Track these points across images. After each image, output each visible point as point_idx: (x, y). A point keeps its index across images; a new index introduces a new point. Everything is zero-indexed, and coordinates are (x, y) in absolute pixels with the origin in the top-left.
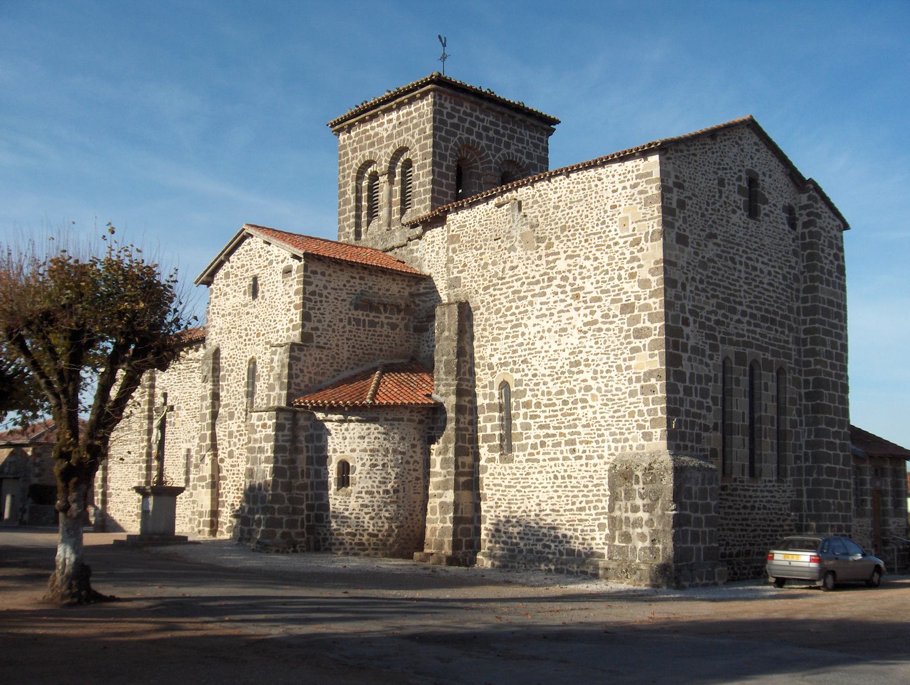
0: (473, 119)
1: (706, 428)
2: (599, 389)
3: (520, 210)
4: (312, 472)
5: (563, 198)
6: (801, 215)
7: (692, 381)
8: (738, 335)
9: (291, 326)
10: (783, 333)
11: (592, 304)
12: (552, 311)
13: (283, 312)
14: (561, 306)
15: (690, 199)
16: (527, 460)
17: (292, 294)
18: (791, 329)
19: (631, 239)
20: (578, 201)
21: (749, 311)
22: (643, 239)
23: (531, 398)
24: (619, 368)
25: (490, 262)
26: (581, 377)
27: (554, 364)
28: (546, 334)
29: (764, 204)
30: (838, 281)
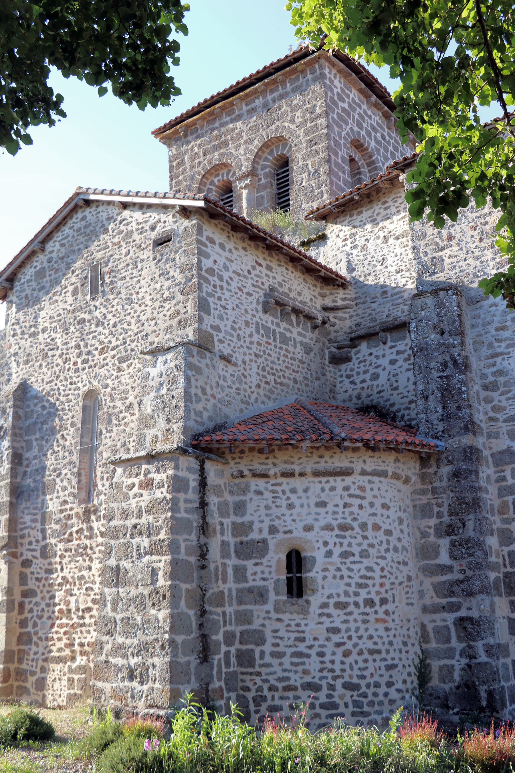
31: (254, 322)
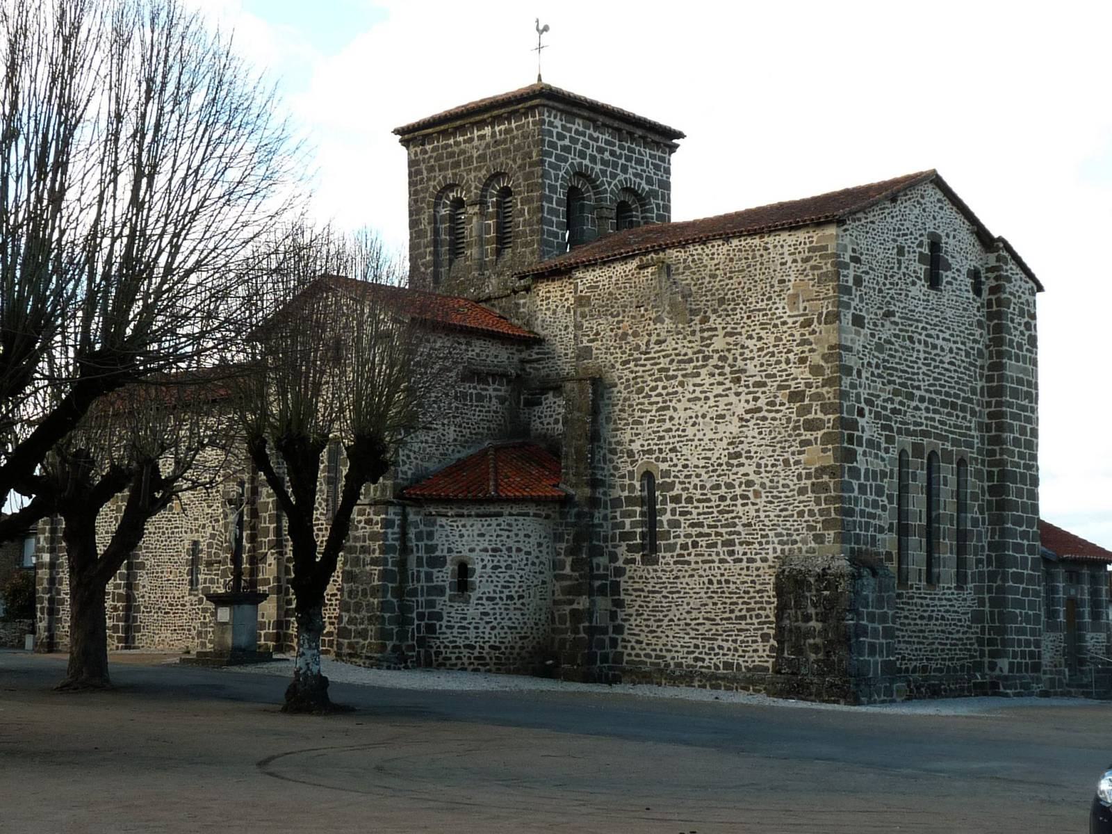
0: (587, 139)
1: (881, 530)
3: (669, 275)
4: (423, 575)
5: (721, 266)
6: (987, 278)
7: (867, 478)
8: (916, 424)
10: (964, 418)
11: (756, 389)
12: (708, 394)
14: (719, 390)
15: (867, 273)
16: (675, 563)
18: (973, 413)
19: (802, 319)
20: (739, 271)
21: (927, 395)
22: (815, 320)
23: (680, 492)
25: (630, 332)
26: (742, 470)
27: (709, 454)
29: (946, 271)
30: (1029, 354)
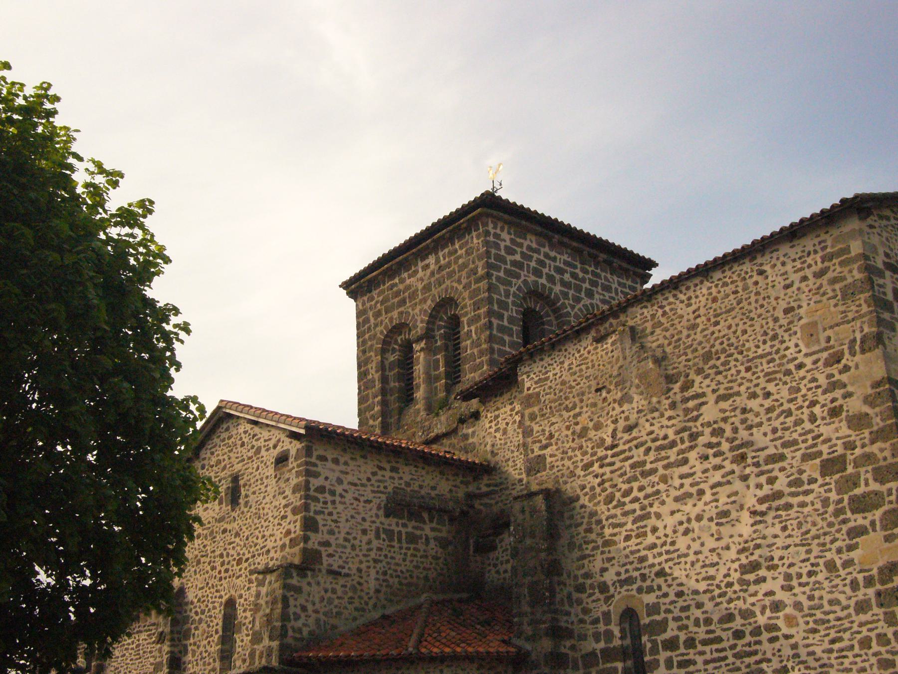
0: (542, 257)
2: (798, 606)
5: (702, 311)
9: (287, 541)
11: (770, 467)
12: (702, 486)
13: (276, 521)
14: (717, 477)
17: (288, 492)
19: (825, 355)
20: (729, 311)
22: (846, 352)
23: (676, 633)
24: (831, 566)
25: (591, 425)
26: (764, 588)
27: (712, 571)
28: (694, 525)
31: (373, 528)
